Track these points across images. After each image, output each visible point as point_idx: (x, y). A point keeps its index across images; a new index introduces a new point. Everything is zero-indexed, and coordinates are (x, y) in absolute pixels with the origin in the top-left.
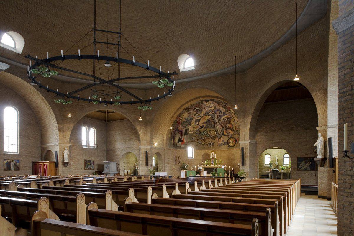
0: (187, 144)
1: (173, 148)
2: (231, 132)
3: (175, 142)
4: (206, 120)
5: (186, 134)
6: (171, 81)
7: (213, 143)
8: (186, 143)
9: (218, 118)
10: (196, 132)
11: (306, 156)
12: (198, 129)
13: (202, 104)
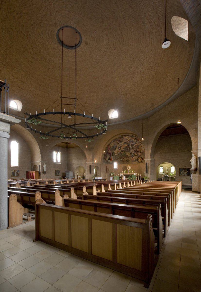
2: (139, 154)
3: (107, 160)
5: (113, 155)
6: (105, 125)
7: (129, 160)
10: (119, 154)
11: (185, 168)
12: (120, 152)
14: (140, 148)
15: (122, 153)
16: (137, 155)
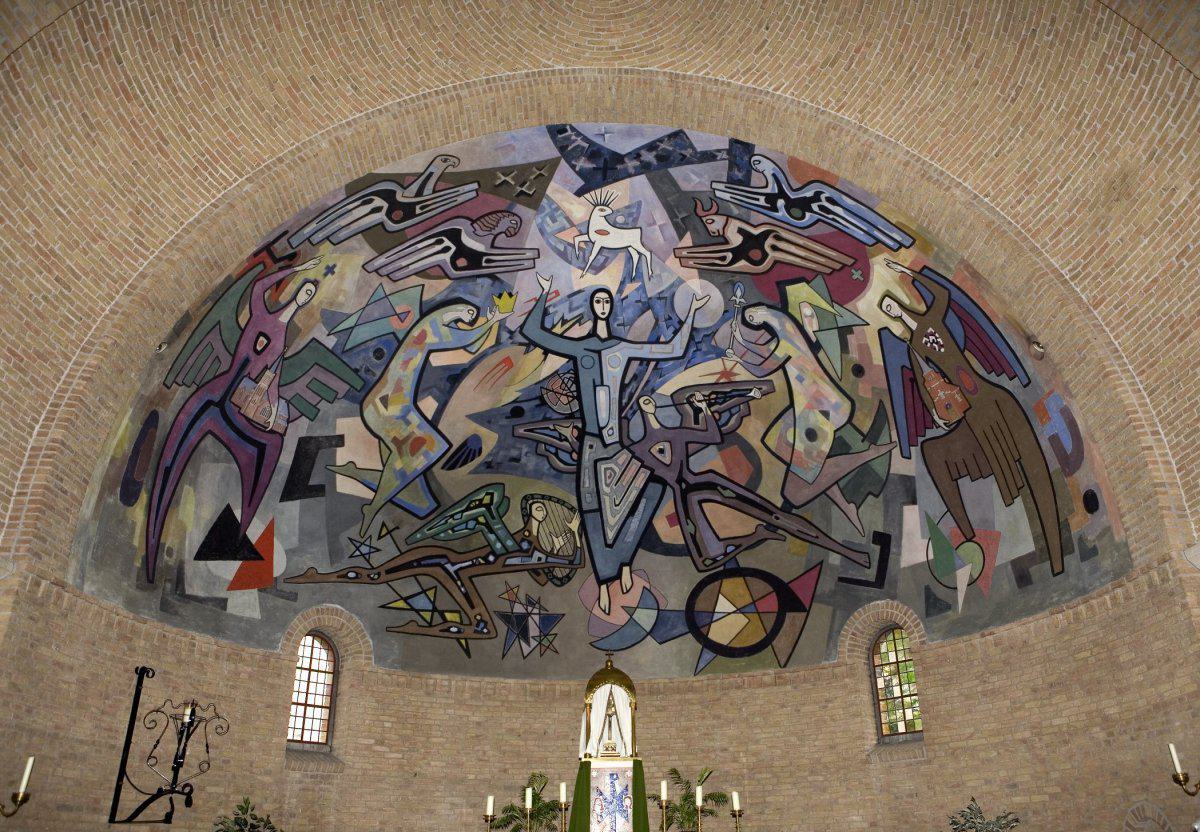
0: (293, 597)
1: (131, 604)
2: (726, 521)
3: (169, 540)
4: (510, 395)
5: (298, 487)
7: (549, 621)
8: (289, 579)
9: (623, 387)
10: (403, 497)
12: (419, 463)
13: (534, 200)
14: (751, 430)
15: (459, 481)
16: (691, 548)
